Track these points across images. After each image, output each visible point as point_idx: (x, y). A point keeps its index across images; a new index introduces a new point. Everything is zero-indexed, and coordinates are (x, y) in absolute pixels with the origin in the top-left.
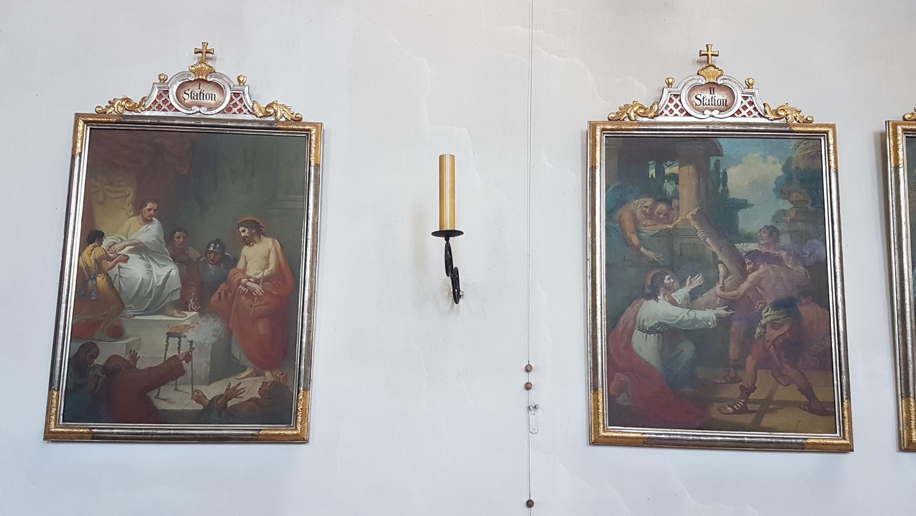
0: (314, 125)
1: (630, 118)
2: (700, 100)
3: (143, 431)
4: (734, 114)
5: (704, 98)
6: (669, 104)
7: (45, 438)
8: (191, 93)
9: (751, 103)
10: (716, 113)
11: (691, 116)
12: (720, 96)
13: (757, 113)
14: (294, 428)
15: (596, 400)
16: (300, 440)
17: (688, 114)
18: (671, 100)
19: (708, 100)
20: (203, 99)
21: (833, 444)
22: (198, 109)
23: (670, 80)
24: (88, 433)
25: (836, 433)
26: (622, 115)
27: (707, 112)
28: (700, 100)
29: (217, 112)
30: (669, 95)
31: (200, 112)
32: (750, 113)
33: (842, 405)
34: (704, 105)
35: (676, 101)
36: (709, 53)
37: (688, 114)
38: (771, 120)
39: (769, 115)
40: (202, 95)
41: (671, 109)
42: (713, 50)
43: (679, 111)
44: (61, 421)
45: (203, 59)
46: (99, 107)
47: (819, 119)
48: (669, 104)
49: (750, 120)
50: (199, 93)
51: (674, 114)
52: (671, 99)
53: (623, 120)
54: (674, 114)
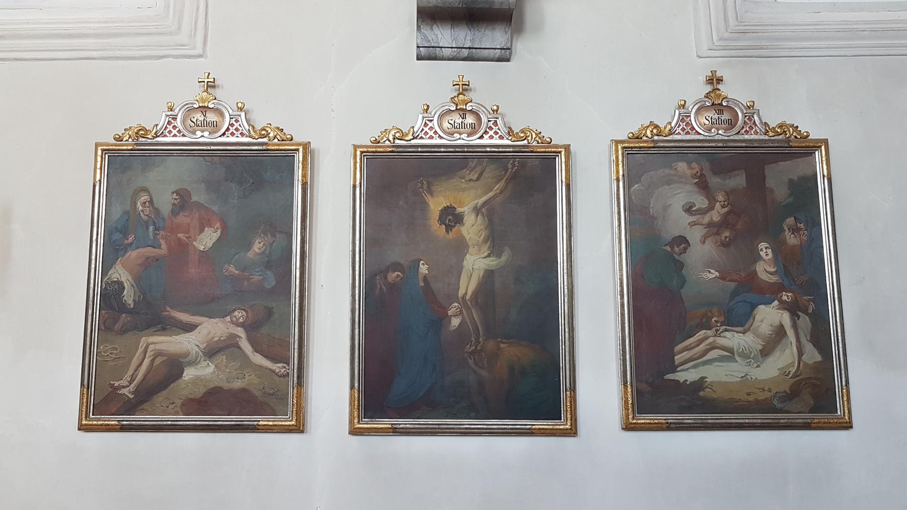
0: (306, 146)
1: (389, 141)
2: (194, 123)
3: (510, 427)
4: (482, 136)
5: (197, 121)
6: (424, 128)
7: (79, 429)
8: (197, 121)
9: (237, 121)
10: (206, 134)
11: (444, 138)
12: (211, 117)
13: (227, 133)
14: (565, 423)
15: (626, 392)
16: (572, 432)
17: (184, 136)
18: (426, 125)
19: (200, 122)
20: (722, 124)
21: (282, 425)
22: (202, 134)
23: (240, 105)
24: (390, 428)
25: (561, 420)
26: (382, 139)
27: (199, 134)
28: (194, 123)
29: (219, 135)
30: (167, 119)
31: (204, 136)
32: (426, 133)
33: (293, 391)
34: (712, 124)
35: (236, 125)
36: (206, 81)
37: (440, 137)
38: (770, 137)
39: (771, 134)
40: (720, 120)
41: (170, 130)
42: (719, 74)
43: (177, 131)
44: (91, 414)
45: (461, 91)
46: (116, 134)
47: (558, 140)
48: (424, 128)
49: (753, 137)
50: (717, 118)
51: (172, 134)
52: (169, 121)
53: (641, 138)
54: (172, 134)
